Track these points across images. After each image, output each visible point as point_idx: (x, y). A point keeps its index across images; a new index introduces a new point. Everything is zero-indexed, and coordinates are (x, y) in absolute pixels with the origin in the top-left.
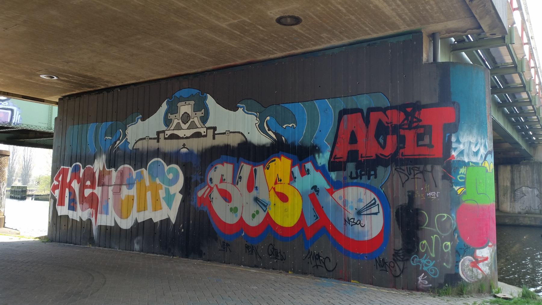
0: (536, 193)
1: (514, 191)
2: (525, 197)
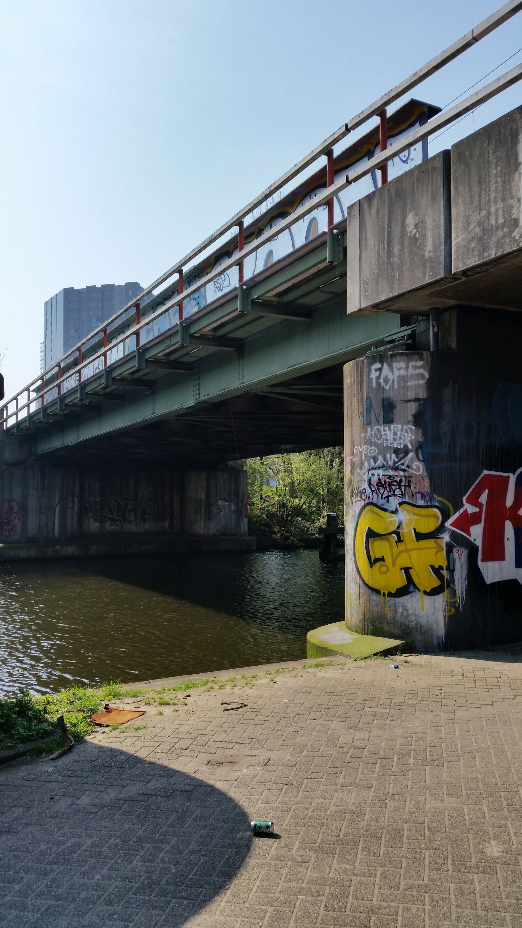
0: (233, 507)
1: (209, 506)
2: (221, 514)
